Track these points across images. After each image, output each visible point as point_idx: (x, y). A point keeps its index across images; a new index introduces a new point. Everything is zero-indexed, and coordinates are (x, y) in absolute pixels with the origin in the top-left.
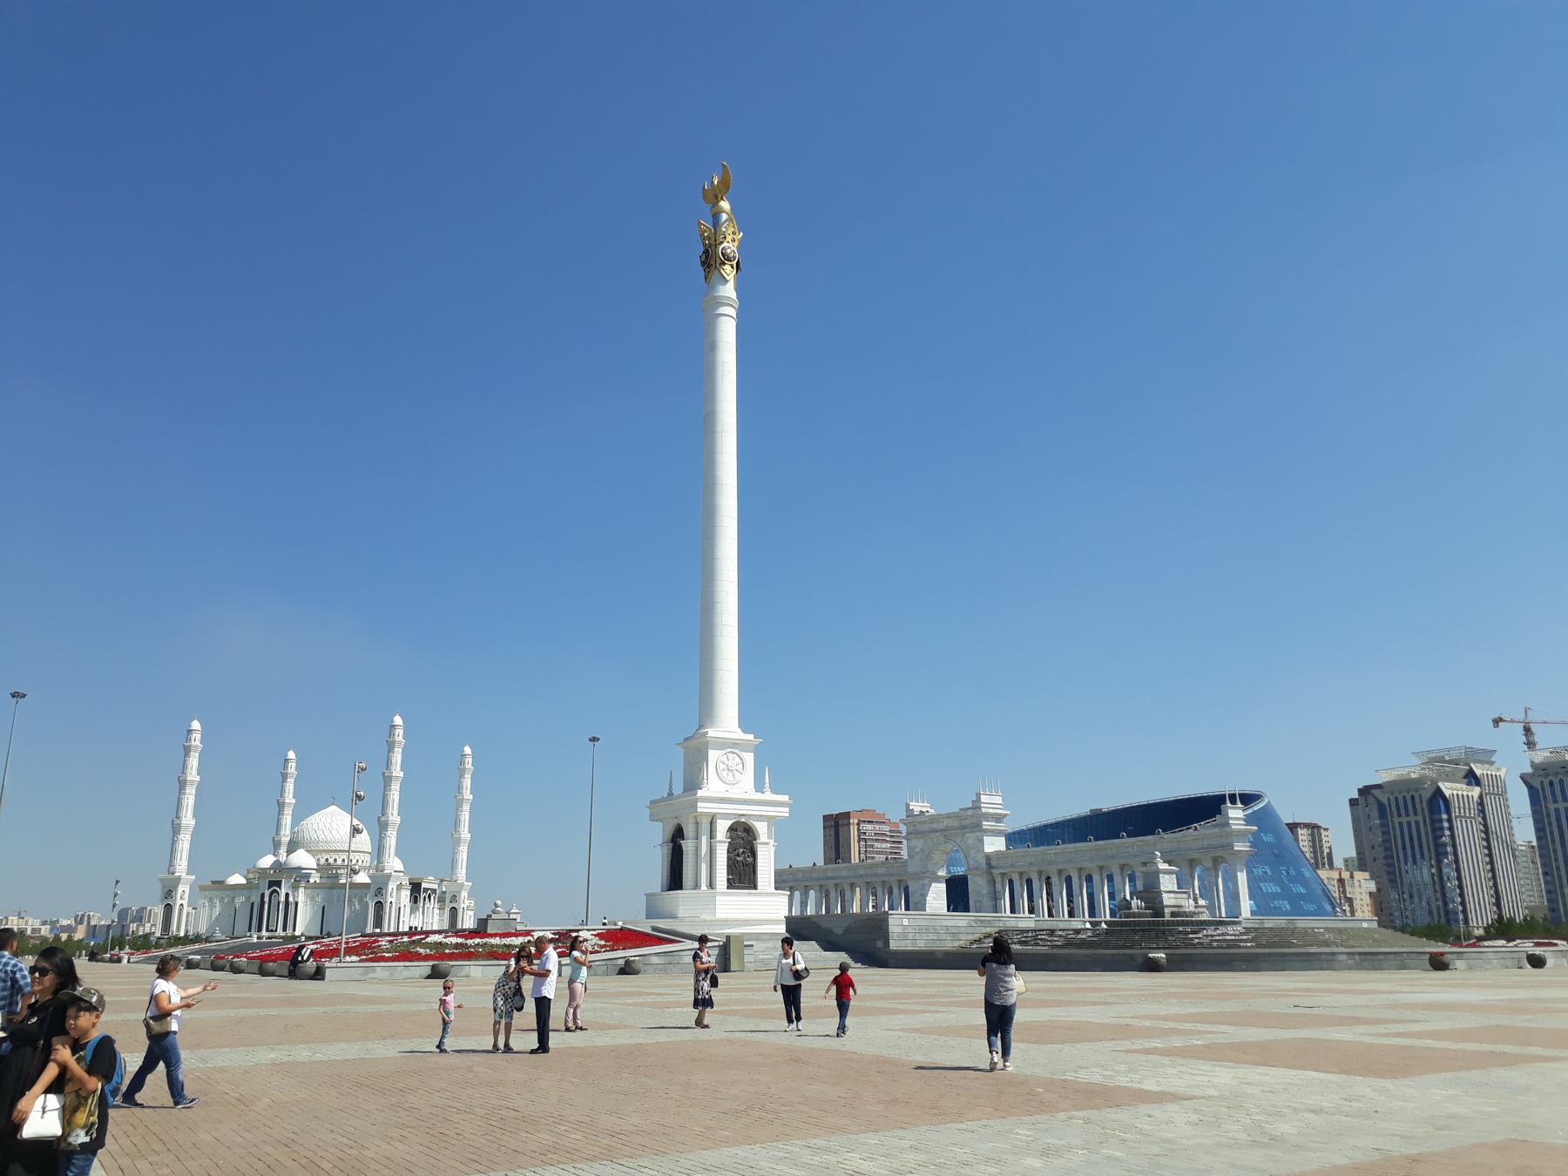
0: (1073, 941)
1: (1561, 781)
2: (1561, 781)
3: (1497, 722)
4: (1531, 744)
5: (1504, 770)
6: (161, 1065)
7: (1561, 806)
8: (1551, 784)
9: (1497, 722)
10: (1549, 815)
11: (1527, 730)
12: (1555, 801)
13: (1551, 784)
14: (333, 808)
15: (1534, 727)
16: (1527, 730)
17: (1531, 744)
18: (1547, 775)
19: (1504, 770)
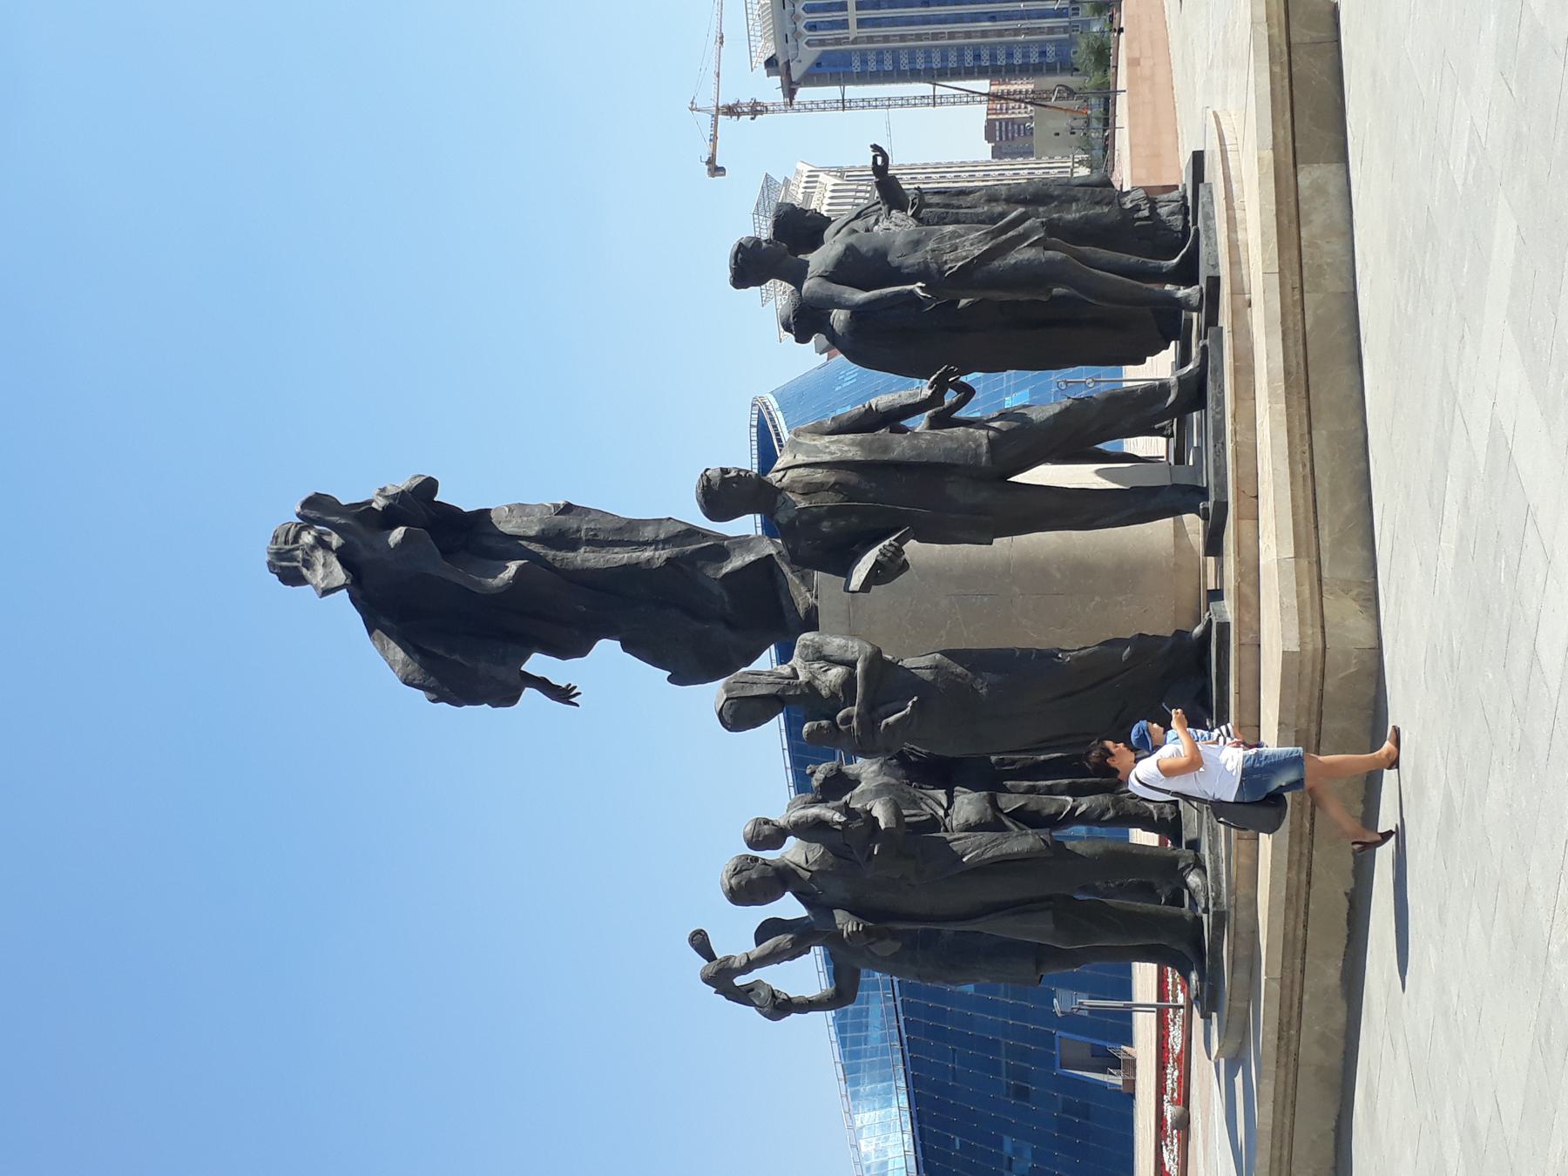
0: (1163, 1164)
1: (810, 9)
2: (810, 9)
3: (715, 170)
4: (756, 110)
5: (800, 166)
6: (956, 415)
7: (852, 15)
8: (812, 27)
9: (715, 170)
10: (870, 39)
11: (731, 111)
12: (844, 24)
13: (812, 27)
14: (344, 502)
15: (727, 99)
16: (731, 111)
17: (756, 110)
18: (797, 34)
19: (800, 166)
